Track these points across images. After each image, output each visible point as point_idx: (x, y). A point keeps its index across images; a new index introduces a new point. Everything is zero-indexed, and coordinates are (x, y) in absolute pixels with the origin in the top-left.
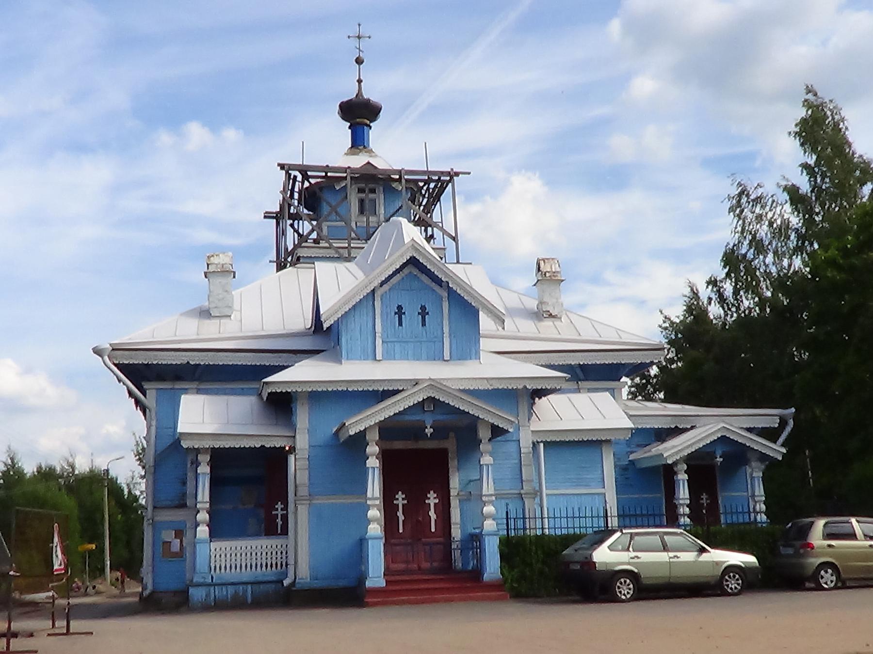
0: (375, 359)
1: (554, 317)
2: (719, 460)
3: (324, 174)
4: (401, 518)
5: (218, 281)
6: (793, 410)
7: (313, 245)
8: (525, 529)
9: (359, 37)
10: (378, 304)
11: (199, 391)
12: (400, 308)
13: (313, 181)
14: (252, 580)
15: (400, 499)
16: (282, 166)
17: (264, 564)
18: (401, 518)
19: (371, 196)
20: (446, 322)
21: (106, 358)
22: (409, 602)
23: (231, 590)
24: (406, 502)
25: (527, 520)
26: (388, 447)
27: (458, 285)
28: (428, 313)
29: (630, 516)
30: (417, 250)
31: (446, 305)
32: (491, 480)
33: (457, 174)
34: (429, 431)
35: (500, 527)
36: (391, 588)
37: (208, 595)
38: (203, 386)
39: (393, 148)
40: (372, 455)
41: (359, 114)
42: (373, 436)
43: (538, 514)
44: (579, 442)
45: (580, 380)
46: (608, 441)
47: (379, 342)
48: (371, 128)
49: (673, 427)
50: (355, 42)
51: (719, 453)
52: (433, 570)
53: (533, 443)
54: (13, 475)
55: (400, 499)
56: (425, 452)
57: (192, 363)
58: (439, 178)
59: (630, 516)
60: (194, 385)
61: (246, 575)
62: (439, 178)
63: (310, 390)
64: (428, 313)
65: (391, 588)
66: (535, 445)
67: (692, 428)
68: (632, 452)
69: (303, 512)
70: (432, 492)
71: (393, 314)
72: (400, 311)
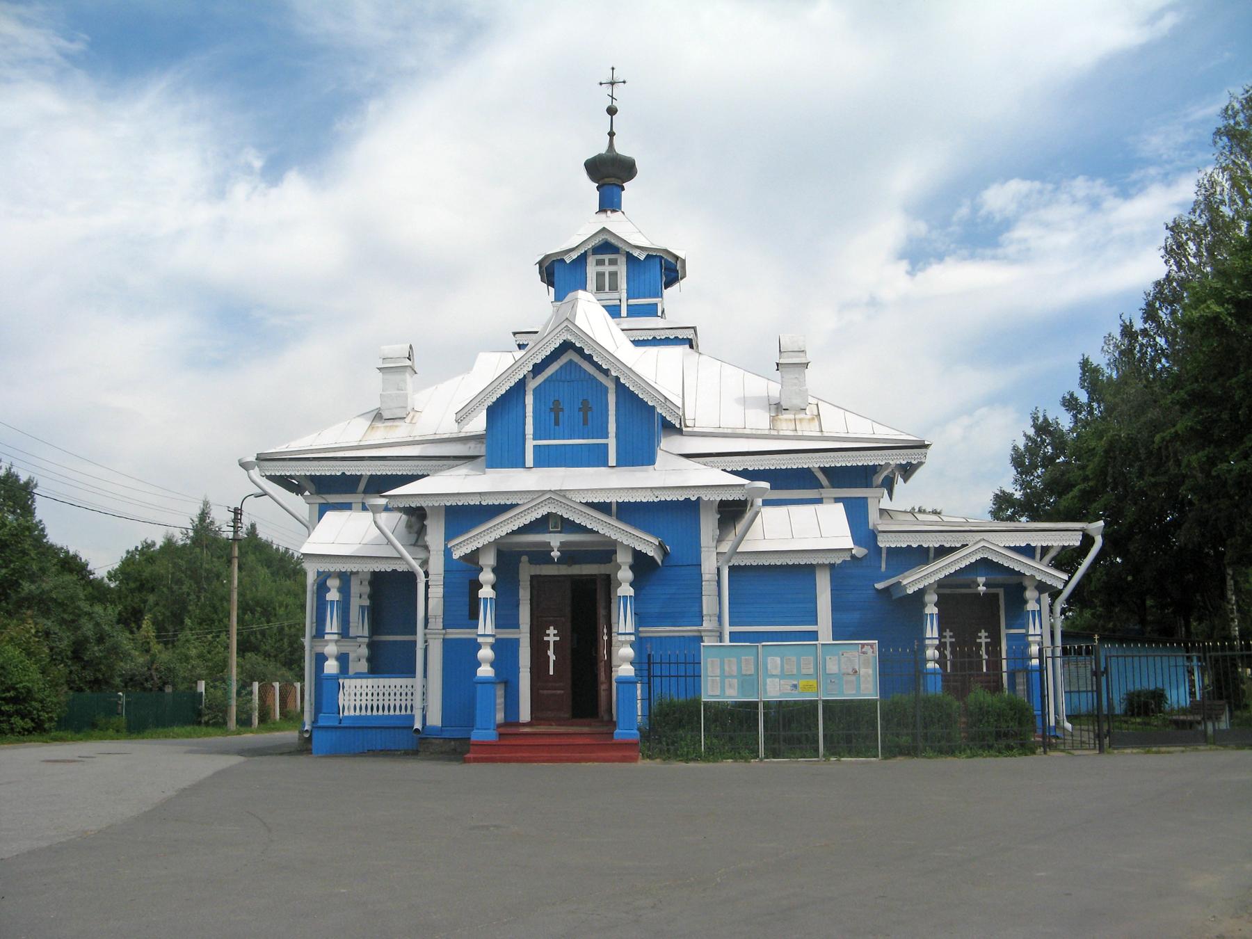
0: (524, 467)
2: (982, 589)
4: (552, 658)
6: (1101, 523)
9: (612, 84)
10: (529, 400)
18: (552, 658)
19: (613, 268)
26: (538, 573)
34: (555, 554)
40: (487, 583)
41: (610, 173)
43: (1059, 661)
48: (623, 189)
50: (607, 90)
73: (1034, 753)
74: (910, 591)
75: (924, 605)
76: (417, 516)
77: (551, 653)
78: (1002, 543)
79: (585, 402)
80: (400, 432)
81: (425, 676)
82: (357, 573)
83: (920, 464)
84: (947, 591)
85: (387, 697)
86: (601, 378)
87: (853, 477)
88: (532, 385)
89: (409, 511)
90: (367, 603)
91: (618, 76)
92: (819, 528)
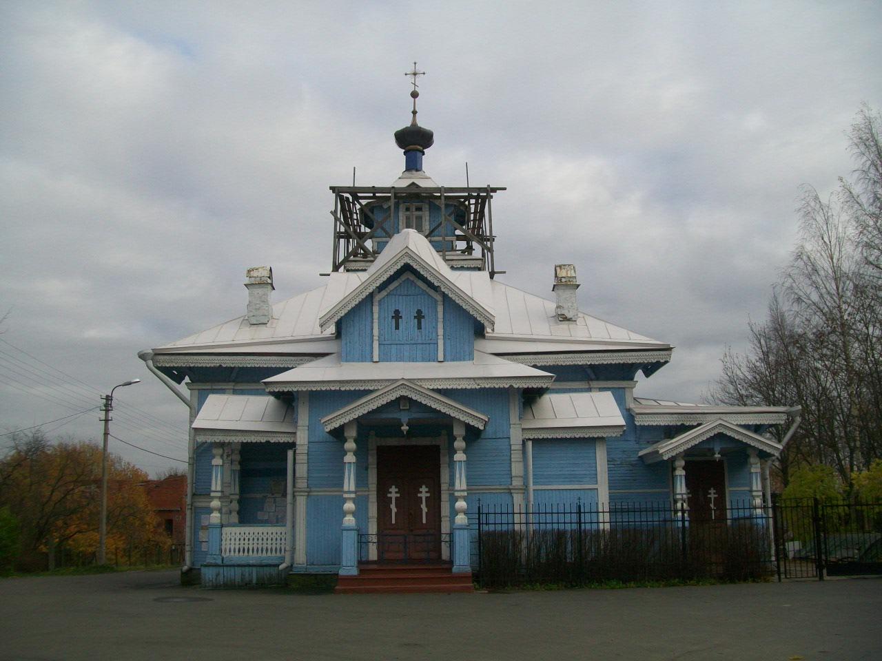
1: (569, 320)
2: (717, 456)
3: (372, 195)
4: (425, 510)
5: (259, 291)
7: (362, 259)
8: (580, 523)
9: (415, 74)
11: (235, 392)
12: (397, 312)
13: (364, 202)
14: (259, 562)
15: (393, 493)
16: (333, 189)
17: (251, 549)
18: (425, 510)
20: (440, 325)
21: (150, 363)
22: (421, 591)
23: (239, 570)
24: (398, 495)
25: (582, 515)
27: (451, 289)
28: (401, 317)
29: (622, 511)
30: (411, 257)
31: (440, 309)
32: (463, 475)
33: (494, 190)
34: (405, 428)
35: (471, 521)
36: (366, 576)
37: (218, 575)
38: (239, 387)
39: (442, 169)
41: (414, 141)
42: (352, 433)
44: (570, 439)
45: (592, 380)
46: (601, 439)
47: (376, 344)
48: (423, 154)
49: (679, 424)
50: (411, 79)
51: (717, 448)
52: (408, 559)
53: (523, 441)
54: (4, 464)
55: (393, 493)
56: (406, 447)
57: (224, 366)
58: (478, 195)
59: (622, 511)
60: (231, 386)
61: (253, 557)
62: (478, 195)
63: (526, 387)
64: (401, 317)
65: (366, 576)
66: (524, 443)
67: (699, 425)
68: (641, 449)
69: (301, 501)
70: (424, 487)
71: (426, 317)
72: (397, 316)
73: (766, 581)
74: (665, 458)
75: (674, 469)
76: (288, 400)
77: (423, 506)
78: (735, 423)
79: (419, 312)
80: (263, 334)
81: (857, 578)
82: (229, 443)
83: (666, 362)
84: (691, 459)
85: (260, 541)
86: (432, 292)
87: (611, 372)
88: (377, 298)
89: (277, 395)
90: (238, 467)
91: (419, 69)
92: (594, 409)
